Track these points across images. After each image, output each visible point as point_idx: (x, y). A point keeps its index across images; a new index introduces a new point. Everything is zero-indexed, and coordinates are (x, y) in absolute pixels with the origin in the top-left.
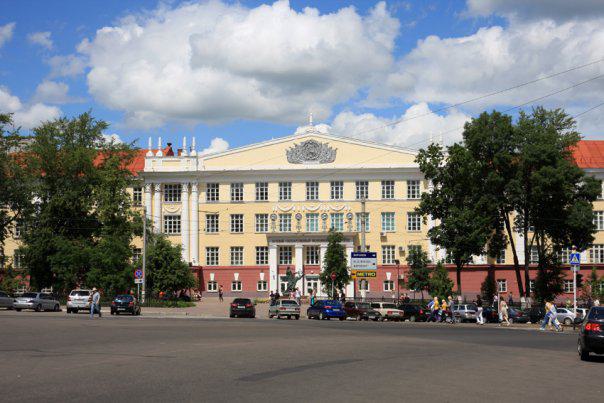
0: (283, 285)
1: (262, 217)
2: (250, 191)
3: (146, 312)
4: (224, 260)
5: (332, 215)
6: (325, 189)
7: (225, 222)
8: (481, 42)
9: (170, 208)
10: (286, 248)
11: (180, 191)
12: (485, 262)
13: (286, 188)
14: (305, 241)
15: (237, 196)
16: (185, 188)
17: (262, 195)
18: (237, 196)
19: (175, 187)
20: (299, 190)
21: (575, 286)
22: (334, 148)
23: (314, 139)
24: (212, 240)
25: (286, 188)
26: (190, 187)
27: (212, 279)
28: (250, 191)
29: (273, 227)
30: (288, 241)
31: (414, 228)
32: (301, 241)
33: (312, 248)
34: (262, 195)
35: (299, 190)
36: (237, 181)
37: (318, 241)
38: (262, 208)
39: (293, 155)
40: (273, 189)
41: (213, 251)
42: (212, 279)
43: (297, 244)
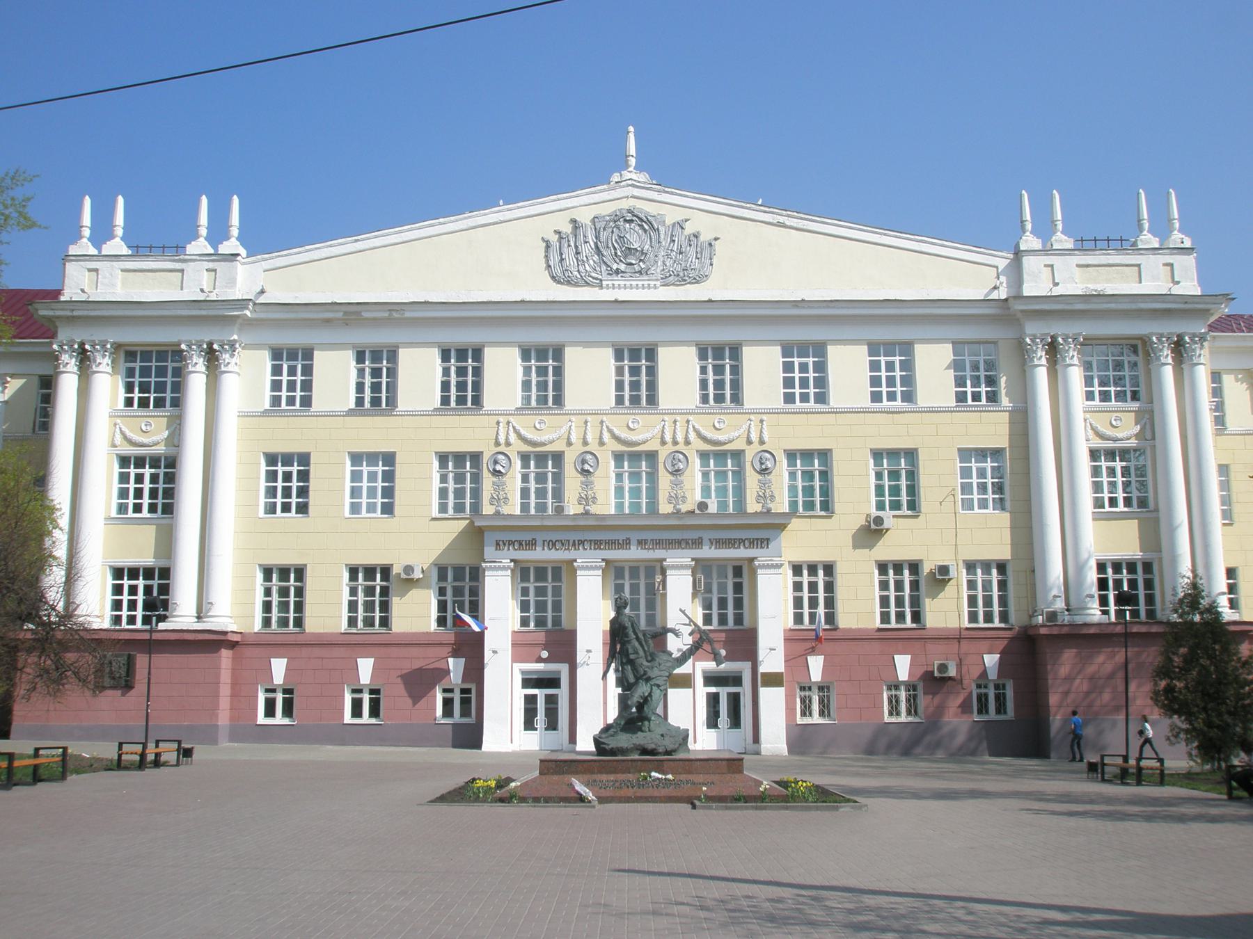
1: (460, 464)
2: (421, 373)
3: (225, 744)
4: (329, 609)
5: (791, 455)
6: (679, 370)
7: (332, 482)
9: (880, 513)
11: (178, 372)
13: (545, 364)
15: (378, 394)
16: (197, 365)
17: (464, 392)
18: (378, 394)
19: (162, 355)
20: (591, 372)
22: (705, 237)
23: (639, 204)
24: (289, 540)
25: (545, 364)
26: (84, 358)
27: (279, 677)
28: (421, 373)
29: (508, 496)
30: (552, 544)
31: (719, 399)
32: (597, 544)
33: (634, 572)
34: (464, 392)
35: (591, 372)
36: (375, 339)
37: (658, 544)
38: (466, 432)
39: (558, 256)
40: (504, 371)
41: (287, 581)
42: (279, 677)
43: (583, 557)
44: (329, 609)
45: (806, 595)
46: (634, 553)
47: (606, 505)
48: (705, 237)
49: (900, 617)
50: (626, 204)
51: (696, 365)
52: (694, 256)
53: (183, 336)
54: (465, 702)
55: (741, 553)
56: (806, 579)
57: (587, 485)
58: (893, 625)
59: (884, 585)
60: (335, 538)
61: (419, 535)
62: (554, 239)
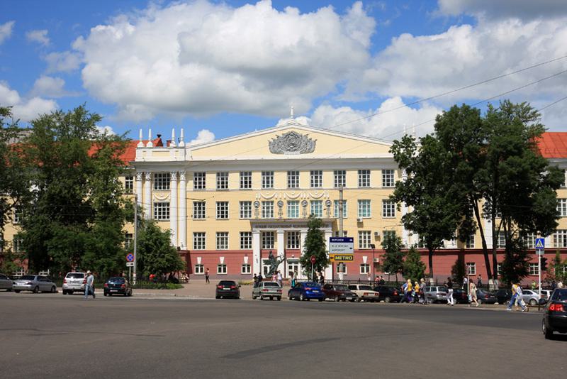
0: (266, 268)
1: (246, 205)
4: (211, 244)
7: (211, 209)
11: (169, 180)
14: (287, 226)
15: (223, 185)
17: (246, 184)
18: (223, 185)
19: (164, 175)
20: (280, 179)
22: (313, 139)
23: (296, 131)
24: (199, 226)
25: (268, 176)
26: (178, 175)
27: (246, 262)
29: (257, 214)
32: (282, 227)
33: (293, 233)
34: (246, 184)
35: (280, 179)
37: (299, 226)
38: (246, 196)
40: (257, 178)
41: (200, 236)
44: (211, 244)
45: (363, 239)
46: (292, 229)
47: (285, 216)
48: (313, 139)
49: (365, 246)
50: (290, 130)
51: (358, 175)
52: (310, 145)
53: (170, 170)
54: (249, 268)
55: (298, 229)
56: (363, 235)
57: (280, 210)
58: (363, 248)
59: (361, 237)
60: (211, 225)
61: (236, 225)
62: (272, 141)
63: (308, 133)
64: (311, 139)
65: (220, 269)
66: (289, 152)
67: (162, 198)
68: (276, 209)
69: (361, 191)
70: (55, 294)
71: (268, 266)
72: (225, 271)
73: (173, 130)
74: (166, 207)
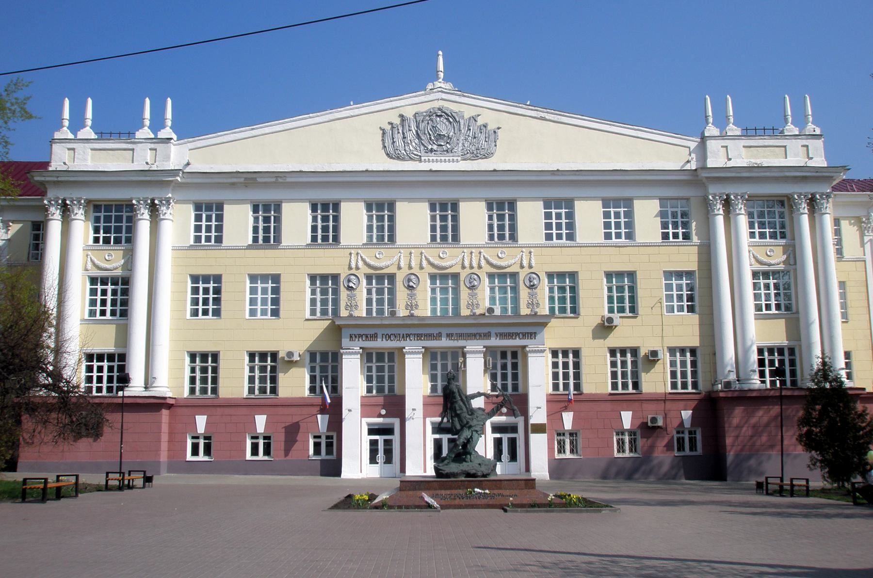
0: (438, 444)
1: (326, 283)
2: (297, 219)
4: (236, 381)
6: (474, 217)
7: (237, 294)
8: (821, 157)
10: (380, 356)
11: (130, 219)
12: (819, 161)
13: (383, 215)
14: (429, 336)
15: (268, 234)
17: (327, 232)
18: (268, 234)
19: (119, 208)
20: (414, 219)
21: (500, 491)
24: (208, 335)
25: (383, 215)
27: (201, 428)
28: (297, 219)
29: (358, 304)
30: (388, 337)
32: (419, 337)
34: (327, 232)
35: (414, 219)
36: (266, 196)
37: (461, 336)
38: (328, 261)
39: (389, 137)
40: (354, 219)
41: (206, 363)
42: (201, 428)
43: (410, 346)
44: (236, 381)
47: (425, 310)
50: (437, 104)
51: (485, 214)
52: (484, 140)
53: (134, 195)
55: (461, 343)
56: (561, 360)
58: (620, 391)
59: (613, 364)
60: (237, 335)
61: (296, 331)
63: (478, 111)
64: (485, 126)
65: (621, 443)
66: (432, 157)
67: (108, 266)
68: (402, 294)
69: (261, 253)
70: (559, 493)
71: (445, 438)
72: (267, 452)
73: (67, 102)
74: (211, 285)
